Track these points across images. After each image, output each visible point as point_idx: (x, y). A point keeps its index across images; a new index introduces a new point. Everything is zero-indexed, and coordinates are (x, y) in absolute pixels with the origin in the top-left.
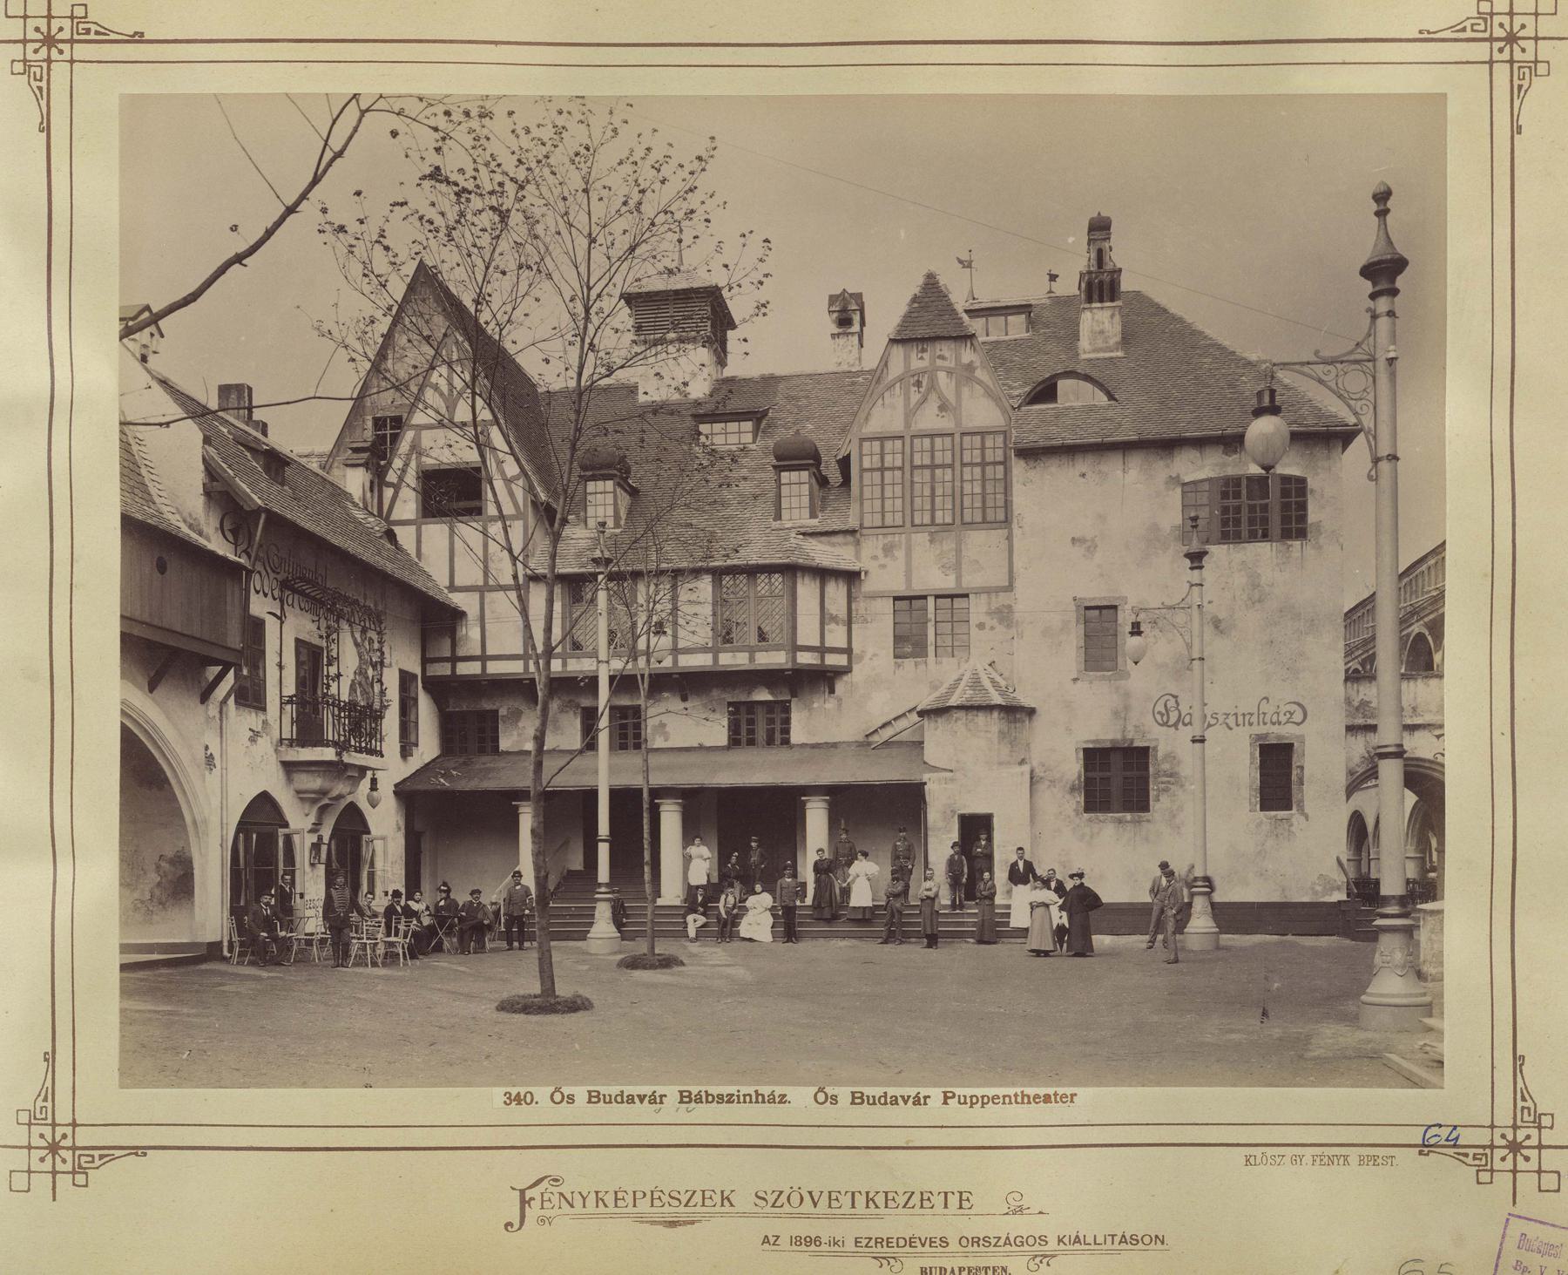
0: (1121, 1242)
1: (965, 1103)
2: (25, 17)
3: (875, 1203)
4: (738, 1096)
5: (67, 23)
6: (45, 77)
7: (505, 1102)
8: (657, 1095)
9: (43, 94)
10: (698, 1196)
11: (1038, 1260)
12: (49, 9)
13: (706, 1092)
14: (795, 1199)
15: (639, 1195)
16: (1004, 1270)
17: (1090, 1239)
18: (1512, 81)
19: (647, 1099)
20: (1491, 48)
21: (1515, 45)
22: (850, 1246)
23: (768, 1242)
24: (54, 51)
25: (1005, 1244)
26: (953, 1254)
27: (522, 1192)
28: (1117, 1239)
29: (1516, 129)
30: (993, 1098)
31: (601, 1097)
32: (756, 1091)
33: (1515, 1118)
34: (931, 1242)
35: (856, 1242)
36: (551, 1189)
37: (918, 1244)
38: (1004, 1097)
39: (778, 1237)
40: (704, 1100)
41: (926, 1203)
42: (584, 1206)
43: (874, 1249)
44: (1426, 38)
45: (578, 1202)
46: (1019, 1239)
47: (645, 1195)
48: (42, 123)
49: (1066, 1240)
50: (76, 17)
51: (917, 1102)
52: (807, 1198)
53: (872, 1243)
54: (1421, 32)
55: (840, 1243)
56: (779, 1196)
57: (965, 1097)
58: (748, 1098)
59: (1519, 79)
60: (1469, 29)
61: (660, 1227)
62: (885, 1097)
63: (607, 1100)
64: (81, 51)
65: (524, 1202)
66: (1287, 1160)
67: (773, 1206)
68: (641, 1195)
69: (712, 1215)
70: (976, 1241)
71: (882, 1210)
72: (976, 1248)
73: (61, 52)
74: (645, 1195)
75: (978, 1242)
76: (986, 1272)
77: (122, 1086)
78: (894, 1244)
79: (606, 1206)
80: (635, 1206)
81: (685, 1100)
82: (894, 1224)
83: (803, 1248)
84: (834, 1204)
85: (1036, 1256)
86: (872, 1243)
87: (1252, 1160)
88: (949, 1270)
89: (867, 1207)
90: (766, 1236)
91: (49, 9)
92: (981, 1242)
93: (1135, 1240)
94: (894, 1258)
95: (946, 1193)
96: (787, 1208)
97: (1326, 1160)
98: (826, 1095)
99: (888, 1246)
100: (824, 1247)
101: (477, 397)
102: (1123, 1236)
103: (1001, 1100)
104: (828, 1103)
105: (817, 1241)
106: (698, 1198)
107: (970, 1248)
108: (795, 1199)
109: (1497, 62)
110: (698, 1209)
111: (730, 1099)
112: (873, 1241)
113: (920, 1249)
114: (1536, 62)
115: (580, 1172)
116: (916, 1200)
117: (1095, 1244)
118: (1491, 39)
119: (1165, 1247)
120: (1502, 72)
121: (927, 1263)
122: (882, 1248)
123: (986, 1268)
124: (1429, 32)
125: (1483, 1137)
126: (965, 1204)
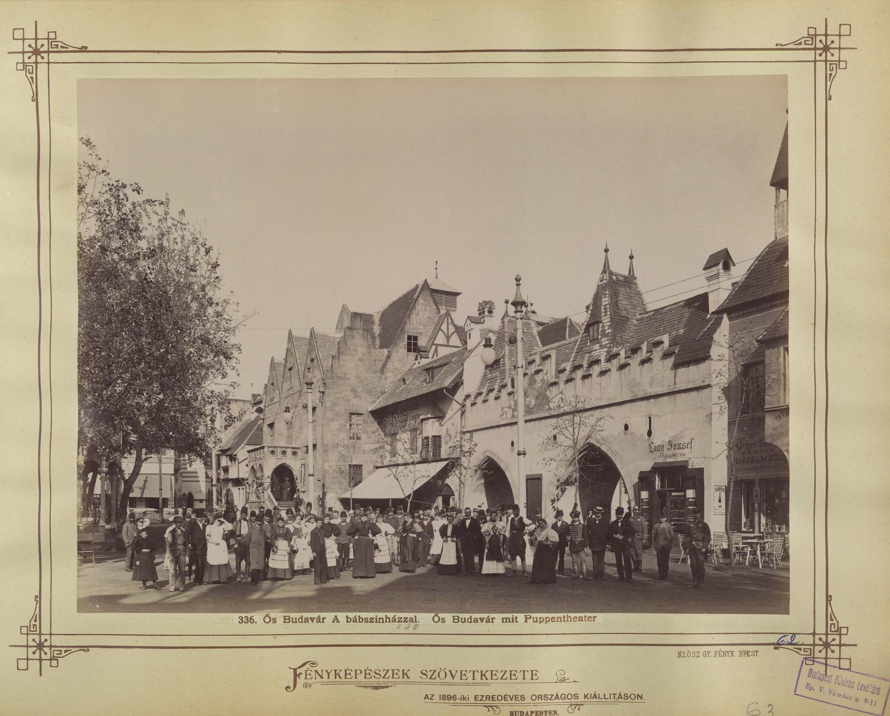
0: (619, 698)
1: (537, 621)
2: (24, 39)
3: (486, 677)
4: (376, 619)
5: (45, 42)
6: (35, 72)
7: (239, 622)
8: (321, 617)
9: (33, 81)
10: (390, 673)
11: (573, 707)
12: (36, 35)
13: (359, 616)
14: (442, 674)
15: (358, 672)
16: (555, 712)
17: (602, 696)
18: (826, 71)
19: (315, 619)
20: (815, 53)
21: (828, 52)
22: (472, 700)
23: (428, 698)
24: (45, 644)
25: (556, 698)
26: (529, 704)
27: (295, 670)
28: (617, 696)
29: (828, 98)
30: (552, 618)
31: (291, 619)
32: (386, 616)
33: (36, 68)
34: (516, 698)
35: (475, 698)
36: (311, 668)
37: (509, 699)
38: (558, 618)
39: (433, 695)
40: (358, 621)
41: (513, 677)
42: (329, 678)
43: (485, 702)
44: (780, 48)
45: (325, 675)
46: (563, 696)
47: (361, 672)
48: (33, 97)
49: (589, 696)
50: (51, 39)
51: (488, 621)
52: (449, 674)
53: (484, 698)
54: (777, 45)
55: (467, 699)
56: (434, 673)
57: (536, 618)
58: (381, 620)
59: (830, 70)
60: (803, 43)
61: (370, 689)
62: (471, 618)
63: (294, 620)
64: (53, 57)
65: (296, 676)
66: (701, 654)
67: (430, 678)
68: (360, 672)
69: (395, 683)
70: (540, 697)
71: (489, 681)
72: (540, 701)
73: (43, 58)
74: (361, 672)
75: (541, 698)
76: (546, 714)
77: (78, 612)
78: (496, 699)
79: (340, 678)
80: (356, 678)
81: (286, 621)
82: (496, 688)
83: (446, 701)
84: (464, 677)
85: (572, 705)
86: (484, 698)
87: (682, 654)
88: (525, 713)
89: (482, 679)
90: (427, 695)
91: (36, 35)
92: (543, 698)
93: (627, 697)
94: (496, 706)
95: (524, 671)
96: (438, 680)
97: (722, 654)
98: (270, 618)
99: (505, 700)
100: (458, 701)
101: (127, 477)
102: (620, 694)
103: (556, 620)
104: (440, 622)
105: (454, 697)
106: (390, 674)
107: (537, 701)
108: (442, 674)
109: (819, 61)
110: (390, 680)
111: (372, 620)
112: (484, 698)
113: (510, 701)
114: (839, 61)
115: (327, 660)
116: (508, 675)
117: (605, 698)
118: (815, 49)
119: (642, 701)
120: (821, 66)
121: (514, 709)
122: (490, 702)
123: (546, 712)
124: (781, 45)
125: (809, 640)
126: (534, 677)
